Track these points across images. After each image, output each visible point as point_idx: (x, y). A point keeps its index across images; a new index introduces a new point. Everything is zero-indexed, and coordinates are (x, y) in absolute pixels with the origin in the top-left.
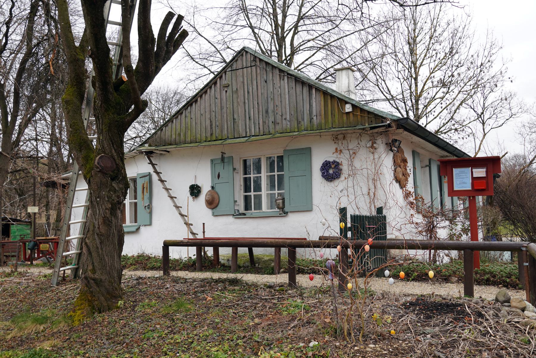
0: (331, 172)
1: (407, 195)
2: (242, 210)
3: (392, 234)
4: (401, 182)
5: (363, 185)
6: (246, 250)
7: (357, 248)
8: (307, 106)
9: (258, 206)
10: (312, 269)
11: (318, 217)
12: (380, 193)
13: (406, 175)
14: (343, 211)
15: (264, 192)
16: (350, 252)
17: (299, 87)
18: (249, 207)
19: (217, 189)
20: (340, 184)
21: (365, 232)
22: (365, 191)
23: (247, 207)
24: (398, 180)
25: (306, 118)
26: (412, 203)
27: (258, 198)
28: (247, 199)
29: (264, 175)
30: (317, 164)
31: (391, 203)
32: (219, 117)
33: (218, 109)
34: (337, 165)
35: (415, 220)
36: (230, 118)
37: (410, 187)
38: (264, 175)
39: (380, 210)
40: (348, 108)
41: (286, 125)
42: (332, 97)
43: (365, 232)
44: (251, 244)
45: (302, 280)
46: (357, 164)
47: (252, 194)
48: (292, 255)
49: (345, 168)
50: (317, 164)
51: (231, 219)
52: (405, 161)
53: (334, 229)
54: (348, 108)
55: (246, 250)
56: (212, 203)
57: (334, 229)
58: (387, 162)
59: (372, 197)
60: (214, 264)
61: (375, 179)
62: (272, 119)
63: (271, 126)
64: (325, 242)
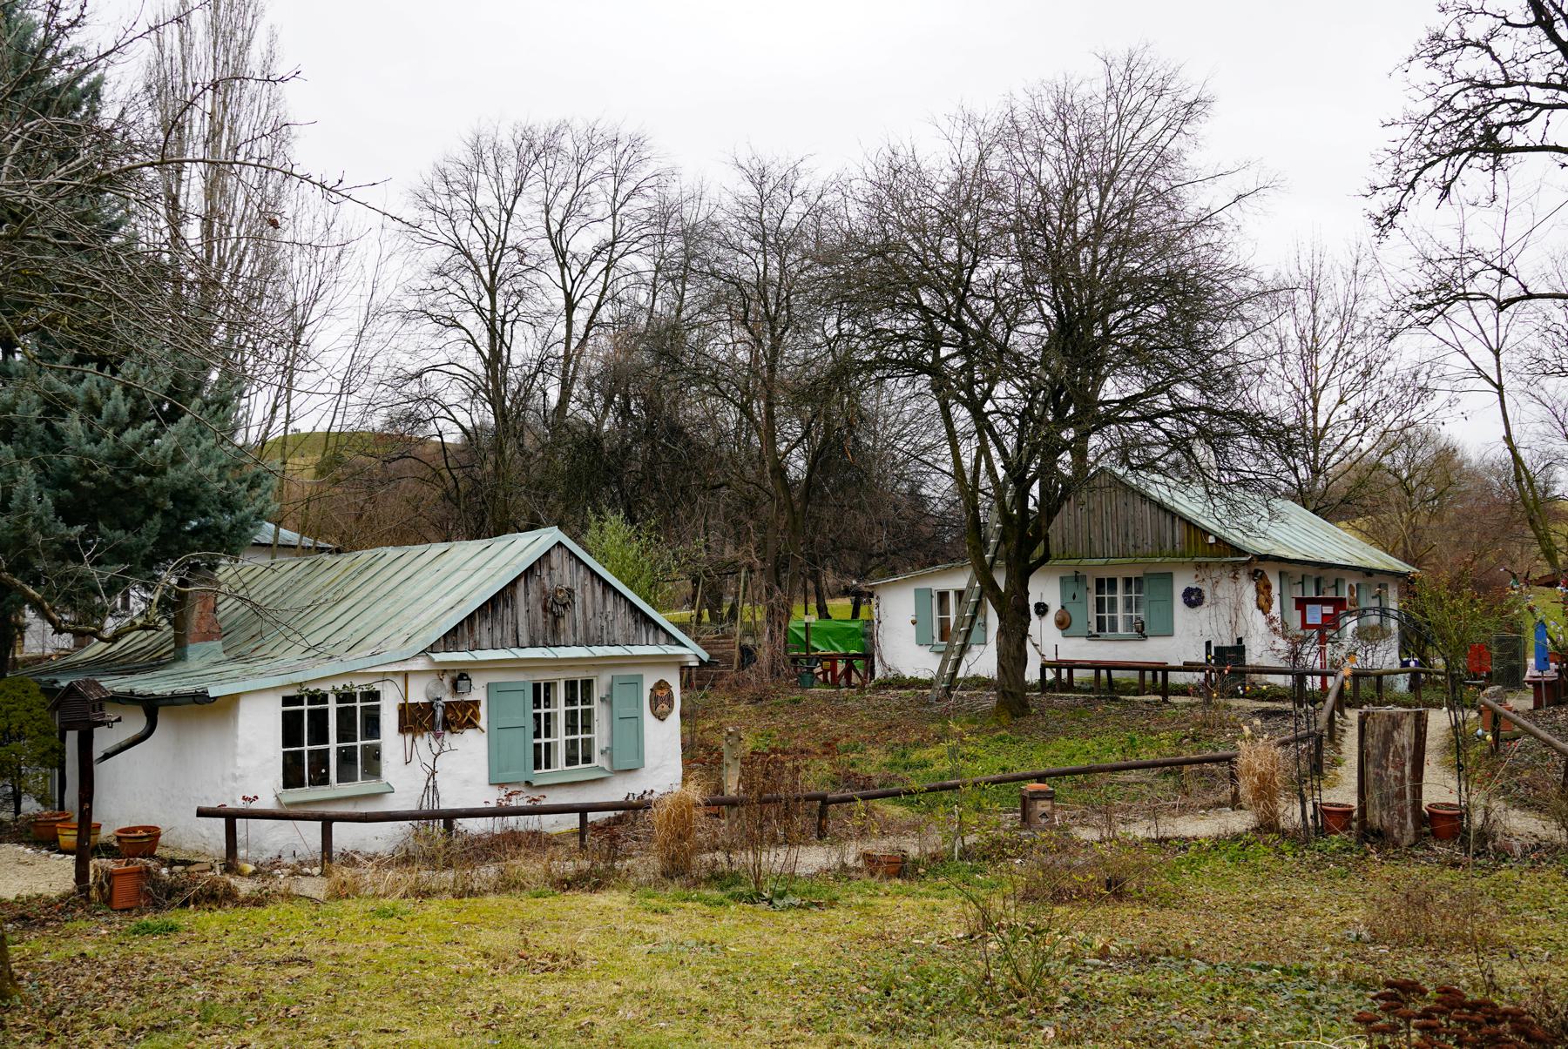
0: (1193, 599)
1: (1272, 620)
2: (1095, 631)
3: (1252, 659)
4: (1264, 607)
5: (1225, 613)
6: (1318, 679)
7: (1220, 672)
8: (1169, 534)
9: (1114, 628)
10: (1183, 691)
11: (1184, 640)
12: (1241, 621)
13: (1269, 601)
14: (1208, 644)
15: (1120, 613)
16: (199, 990)
17: (1161, 514)
18: (1102, 629)
19: (1068, 607)
20: (1203, 612)
21: (1228, 661)
22: (1227, 619)
23: (1101, 627)
24: (1259, 607)
25: (1169, 544)
26: (1275, 629)
27: (1113, 621)
28: (1100, 621)
29: (1120, 595)
30: (1179, 590)
31: (1252, 632)
32: (1073, 534)
33: (1072, 526)
34: (1199, 591)
35: (1277, 647)
36: (1086, 537)
37: (1275, 610)
38: (1120, 595)
39: (1240, 640)
40: (1211, 540)
41: (1148, 549)
42: (1196, 527)
43: (1228, 661)
44: (1110, 666)
45: (1172, 699)
46: (1220, 592)
47: (1107, 615)
48: (1165, 677)
49: (1207, 595)
50: (1179, 590)
51: (1084, 641)
52: (1268, 587)
53: (1199, 656)
54: (1211, 540)
55: (1318, 679)
56: (1063, 624)
57: (1199, 656)
58: (1249, 591)
59: (1234, 624)
60: (1069, 686)
61: (1237, 609)
62: (1131, 542)
63: (1131, 549)
64: (1189, 667)
